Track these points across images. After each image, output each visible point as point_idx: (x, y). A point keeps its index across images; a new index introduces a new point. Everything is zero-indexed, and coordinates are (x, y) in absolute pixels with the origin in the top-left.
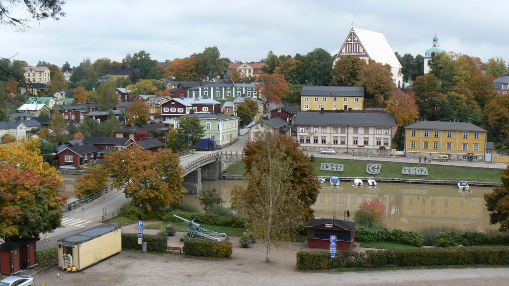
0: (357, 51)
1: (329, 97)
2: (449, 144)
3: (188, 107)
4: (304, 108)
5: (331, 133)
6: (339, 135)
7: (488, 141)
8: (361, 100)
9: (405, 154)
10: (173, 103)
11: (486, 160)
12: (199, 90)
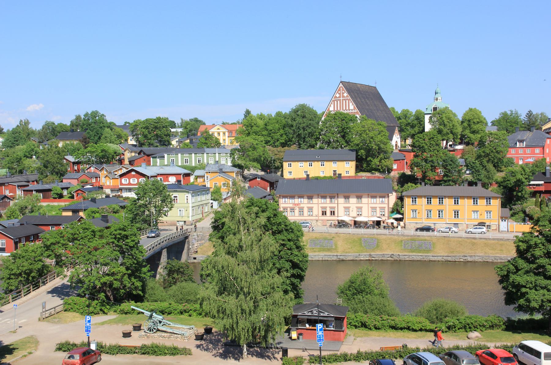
0: (347, 109)
1: (316, 162)
2: (456, 213)
3: (152, 177)
4: (286, 176)
5: (368, 204)
6: (327, 203)
7: (502, 207)
8: (353, 164)
9: (405, 225)
10: (133, 173)
11: (501, 229)
12: (164, 157)
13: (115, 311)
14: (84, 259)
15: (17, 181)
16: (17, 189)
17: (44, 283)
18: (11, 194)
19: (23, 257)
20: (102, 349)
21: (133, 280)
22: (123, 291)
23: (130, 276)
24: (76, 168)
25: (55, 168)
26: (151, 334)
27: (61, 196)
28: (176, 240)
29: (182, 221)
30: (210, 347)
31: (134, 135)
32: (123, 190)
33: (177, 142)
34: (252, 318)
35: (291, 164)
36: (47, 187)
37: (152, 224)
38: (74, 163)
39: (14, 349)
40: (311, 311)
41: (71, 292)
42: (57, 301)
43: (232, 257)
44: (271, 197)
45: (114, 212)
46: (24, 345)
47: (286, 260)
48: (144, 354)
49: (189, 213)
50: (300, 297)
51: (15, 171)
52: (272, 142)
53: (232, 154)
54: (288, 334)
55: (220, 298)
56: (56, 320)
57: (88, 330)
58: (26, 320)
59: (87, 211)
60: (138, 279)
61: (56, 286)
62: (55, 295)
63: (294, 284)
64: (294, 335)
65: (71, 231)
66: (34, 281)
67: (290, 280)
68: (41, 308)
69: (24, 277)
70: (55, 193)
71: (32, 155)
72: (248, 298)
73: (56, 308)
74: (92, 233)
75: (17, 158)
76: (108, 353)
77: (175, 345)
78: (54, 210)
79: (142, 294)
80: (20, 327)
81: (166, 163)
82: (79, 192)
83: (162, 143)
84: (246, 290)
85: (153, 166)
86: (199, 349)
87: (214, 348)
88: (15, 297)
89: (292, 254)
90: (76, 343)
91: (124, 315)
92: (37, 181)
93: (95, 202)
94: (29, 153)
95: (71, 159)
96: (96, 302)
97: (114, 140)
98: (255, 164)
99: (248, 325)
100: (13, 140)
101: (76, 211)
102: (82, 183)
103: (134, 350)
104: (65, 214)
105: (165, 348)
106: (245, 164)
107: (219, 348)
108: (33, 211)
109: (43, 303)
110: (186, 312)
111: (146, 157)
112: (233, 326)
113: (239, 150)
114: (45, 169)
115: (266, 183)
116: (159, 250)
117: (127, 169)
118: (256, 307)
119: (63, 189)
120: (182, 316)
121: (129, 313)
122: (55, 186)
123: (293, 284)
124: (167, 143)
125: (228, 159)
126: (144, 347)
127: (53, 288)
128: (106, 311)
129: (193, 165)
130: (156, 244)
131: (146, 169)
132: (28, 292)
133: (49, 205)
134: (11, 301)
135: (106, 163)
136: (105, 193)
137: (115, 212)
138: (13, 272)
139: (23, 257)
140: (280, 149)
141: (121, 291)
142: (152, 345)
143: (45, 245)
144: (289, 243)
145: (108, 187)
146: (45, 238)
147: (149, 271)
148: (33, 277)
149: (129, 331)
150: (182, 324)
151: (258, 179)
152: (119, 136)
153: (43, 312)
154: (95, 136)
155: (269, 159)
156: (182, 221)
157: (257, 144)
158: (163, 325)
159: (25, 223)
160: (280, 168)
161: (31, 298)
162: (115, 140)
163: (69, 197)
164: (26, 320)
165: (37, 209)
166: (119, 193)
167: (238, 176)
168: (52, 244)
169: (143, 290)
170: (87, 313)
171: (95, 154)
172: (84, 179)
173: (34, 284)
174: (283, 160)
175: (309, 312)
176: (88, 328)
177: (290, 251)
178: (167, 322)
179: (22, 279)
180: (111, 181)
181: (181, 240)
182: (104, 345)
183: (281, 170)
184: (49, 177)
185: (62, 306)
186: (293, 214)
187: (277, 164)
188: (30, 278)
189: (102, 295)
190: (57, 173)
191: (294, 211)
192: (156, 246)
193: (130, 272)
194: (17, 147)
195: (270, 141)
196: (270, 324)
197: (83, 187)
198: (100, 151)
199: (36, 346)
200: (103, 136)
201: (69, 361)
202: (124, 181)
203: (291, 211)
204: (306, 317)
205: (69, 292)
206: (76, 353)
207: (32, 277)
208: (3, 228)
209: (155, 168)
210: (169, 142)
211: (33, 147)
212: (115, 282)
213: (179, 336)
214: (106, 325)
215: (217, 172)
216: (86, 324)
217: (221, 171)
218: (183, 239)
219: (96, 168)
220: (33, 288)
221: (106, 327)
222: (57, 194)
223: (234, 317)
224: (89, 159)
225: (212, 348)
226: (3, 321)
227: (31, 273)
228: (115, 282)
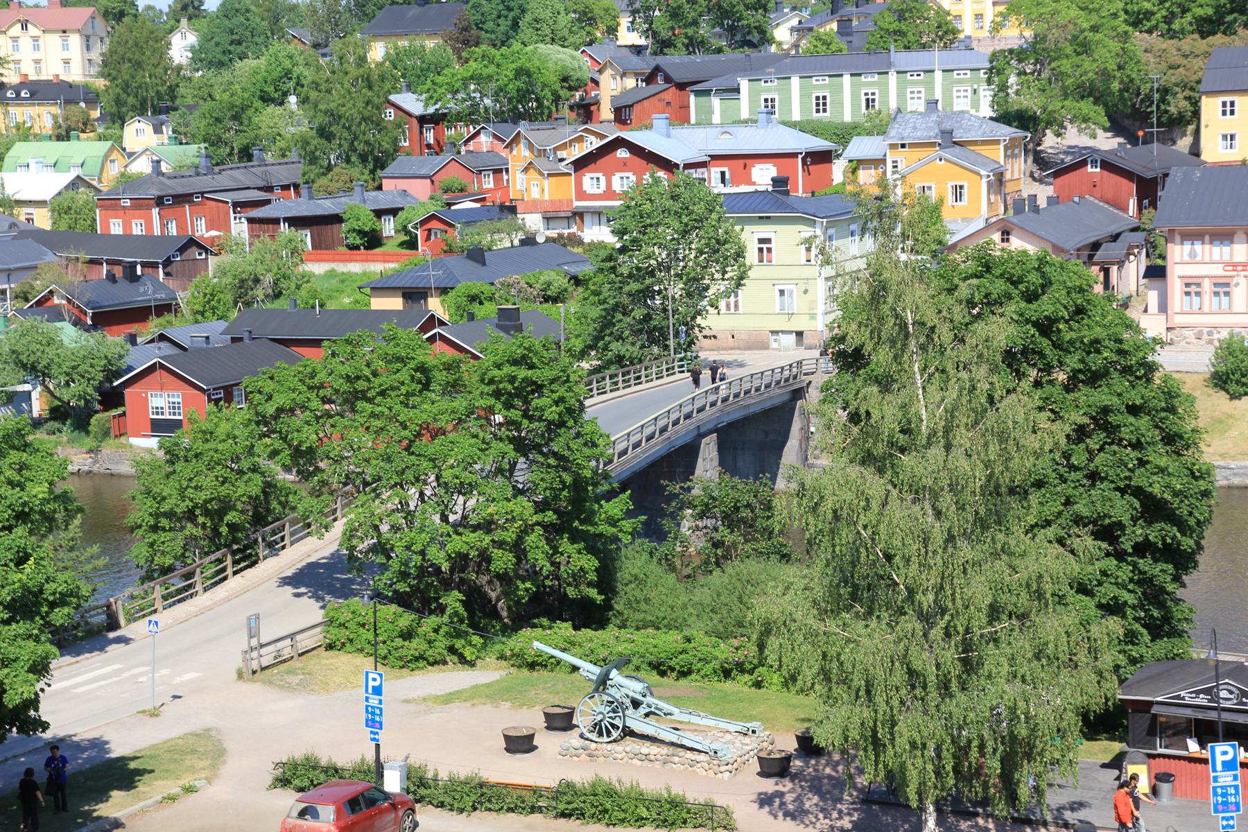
4: (1213, 151)
10: (622, 153)
13: (502, 657)
14: (388, 466)
15: (232, 185)
16: (232, 216)
17: (273, 548)
18: (214, 233)
19: (196, 456)
20: (422, 791)
21: (565, 545)
22: (528, 585)
23: (552, 531)
24: (430, 137)
25: (356, 138)
26: (603, 746)
27: (373, 240)
28: (755, 404)
29: (791, 332)
30: (807, 805)
31: (637, 11)
32: (587, 218)
33: (792, 29)
34: (950, 706)
35: (1232, 104)
36: (326, 206)
37: (672, 343)
38: (423, 120)
39: (140, 772)
40: (1207, 691)
41: (358, 584)
42: (308, 611)
43: (881, 471)
44: (1139, 237)
45: (547, 299)
46: (175, 761)
47: (1117, 489)
48: (563, 815)
49: (814, 302)
50: (1176, 633)
51: (228, 150)
52: (1158, 16)
53: (996, 69)
54: (1116, 772)
55: (832, 626)
56: (294, 680)
57: (373, 720)
58: (199, 674)
59: (452, 294)
60: (582, 545)
61: (313, 559)
62: (303, 590)
63: (1151, 580)
64: (1141, 772)
65: (346, 369)
66: (235, 541)
67: (1135, 565)
68: (244, 634)
69: (204, 526)
70: (354, 230)
71: (285, 94)
72: (937, 633)
73: (299, 637)
74: (418, 375)
75: (232, 106)
76: (441, 805)
77: (677, 791)
78: (348, 290)
79: (599, 598)
80: (175, 697)
81: (745, 114)
82: (434, 224)
83: (738, 37)
84: (927, 600)
85: (698, 124)
86: (767, 809)
87: (822, 810)
88: (179, 591)
89: (1142, 463)
90: (339, 764)
91: (525, 671)
92: (296, 186)
93: (483, 263)
94: (276, 83)
95: (413, 103)
96: (433, 620)
97: (566, 33)
98: (1086, 106)
99: (935, 727)
100: (225, 39)
101: (414, 295)
102: (447, 190)
103: (530, 799)
104: (381, 303)
105: (640, 798)
106: (1044, 109)
107: (840, 812)
108: (280, 293)
109: (249, 619)
110: (743, 671)
111: (671, 95)
112: (875, 732)
113: (1020, 55)
114: (323, 141)
115: (1124, 182)
116: (688, 439)
117: (602, 137)
118: (969, 666)
119: (379, 213)
120: (728, 685)
121: (541, 664)
122: (352, 203)
123: (1145, 581)
124: (755, 36)
125: (982, 93)
126: (566, 790)
127: (299, 566)
128: (468, 653)
129: (848, 118)
130: (674, 417)
131: (668, 136)
132: (219, 578)
133: (333, 270)
134: (159, 605)
135: (530, 117)
136: (522, 228)
137: (555, 300)
138: (165, 507)
139: (196, 456)
140: (1193, 42)
141: (522, 586)
142: (593, 785)
143: (257, 414)
144: (1131, 419)
145: (533, 207)
146: (260, 392)
147: (629, 514)
148: (233, 527)
149: (525, 732)
150: (721, 715)
151: (1089, 169)
152: (585, 13)
153: (252, 649)
154: (499, 17)
155: (1145, 89)
156: (791, 332)
157: (1095, 29)
158: (647, 715)
159: (246, 335)
160: (1189, 123)
161: (227, 600)
162: (571, 32)
163: (402, 244)
164: (199, 674)
165: (293, 286)
166: (574, 230)
167: (1014, 156)
168: (280, 410)
169: (606, 580)
170: (401, 658)
171: (493, 85)
172: (454, 175)
173: (239, 550)
174: (1201, 87)
175: (1198, 693)
176: (373, 714)
177: (1135, 454)
178: (662, 704)
179: (198, 532)
180: (546, 182)
181: (777, 402)
182: (430, 775)
183: (1191, 128)
184: (336, 170)
185: (319, 629)
186: (1225, 306)
187: (1177, 105)
188: (224, 530)
189: (453, 600)
190: (363, 158)
191: (1227, 294)
192: (676, 423)
193: (550, 516)
194: (239, 64)
195: (1153, 14)
196: (1022, 731)
197: (449, 205)
198: (511, 75)
199: (214, 767)
200: (528, 17)
201: (301, 826)
202: (591, 182)
203: (1216, 294)
204: (1188, 713)
205: (352, 581)
206: (324, 801)
207: (227, 525)
208: (176, 351)
209: (701, 132)
210: (762, 31)
211: (287, 64)
212: (496, 553)
213: (702, 757)
214: (457, 704)
215: (933, 145)
216: (367, 699)
217: (948, 140)
218: (786, 398)
219: (495, 137)
220: (235, 562)
221: (457, 710)
222: (361, 233)
223: (880, 700)
224: (475, 106)
225: (814, 809)
226: (127, 674)
227: (226, 514)
228: (496, 553)
